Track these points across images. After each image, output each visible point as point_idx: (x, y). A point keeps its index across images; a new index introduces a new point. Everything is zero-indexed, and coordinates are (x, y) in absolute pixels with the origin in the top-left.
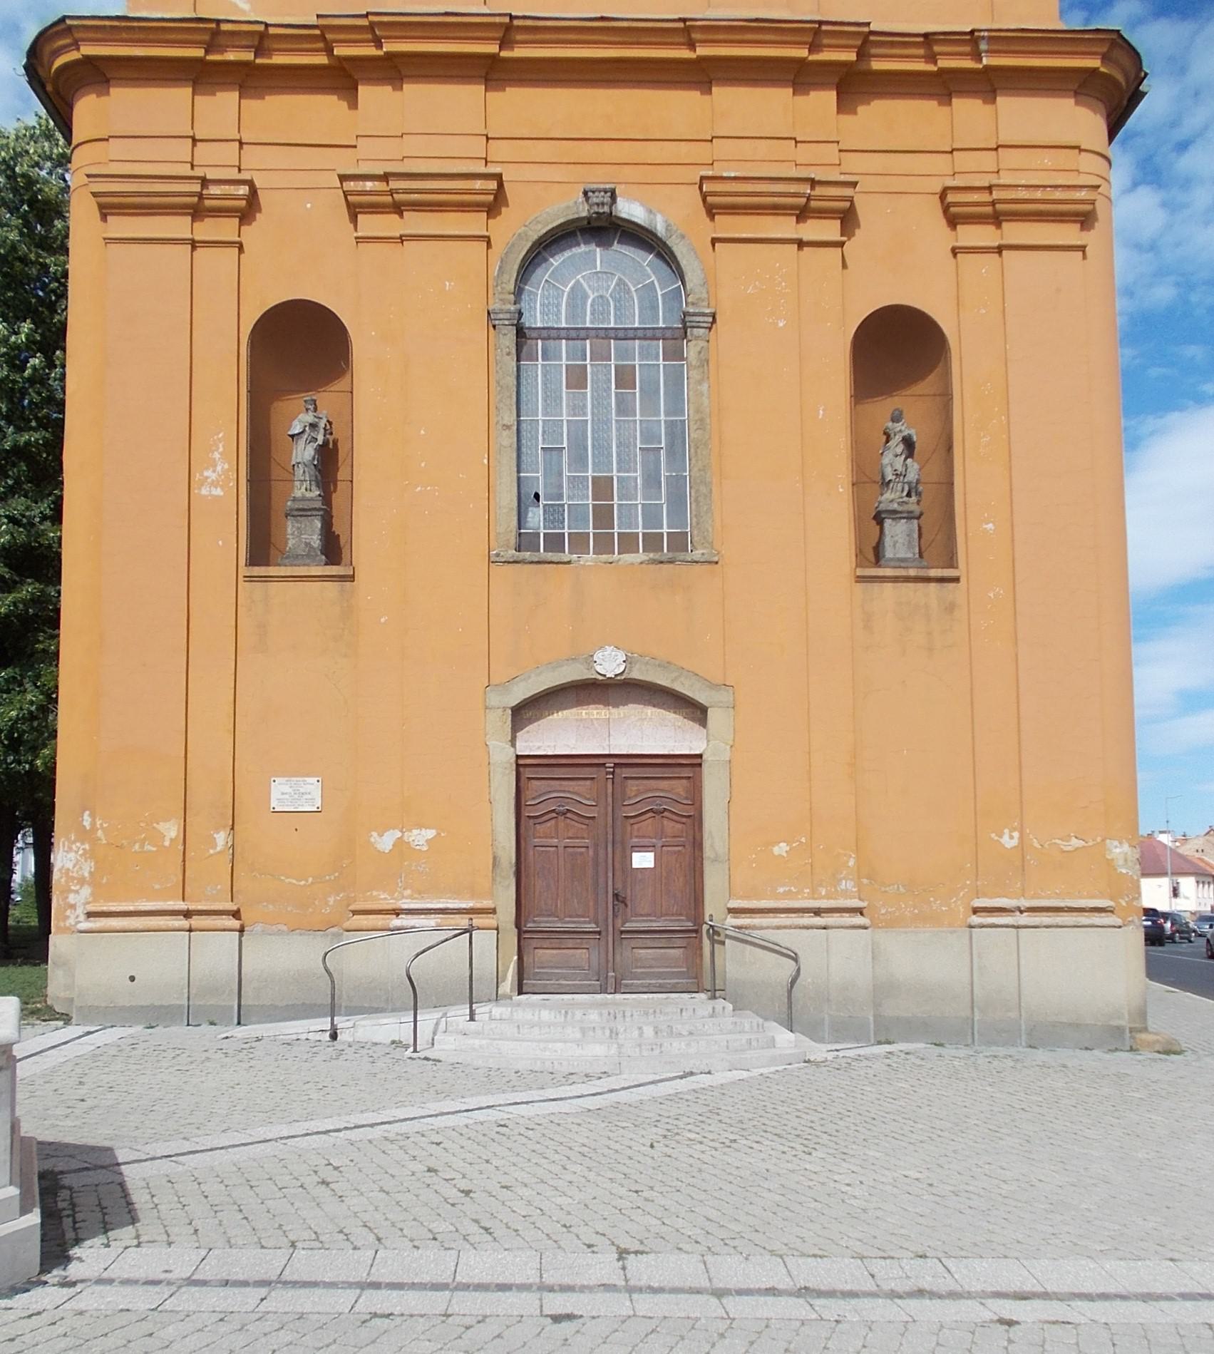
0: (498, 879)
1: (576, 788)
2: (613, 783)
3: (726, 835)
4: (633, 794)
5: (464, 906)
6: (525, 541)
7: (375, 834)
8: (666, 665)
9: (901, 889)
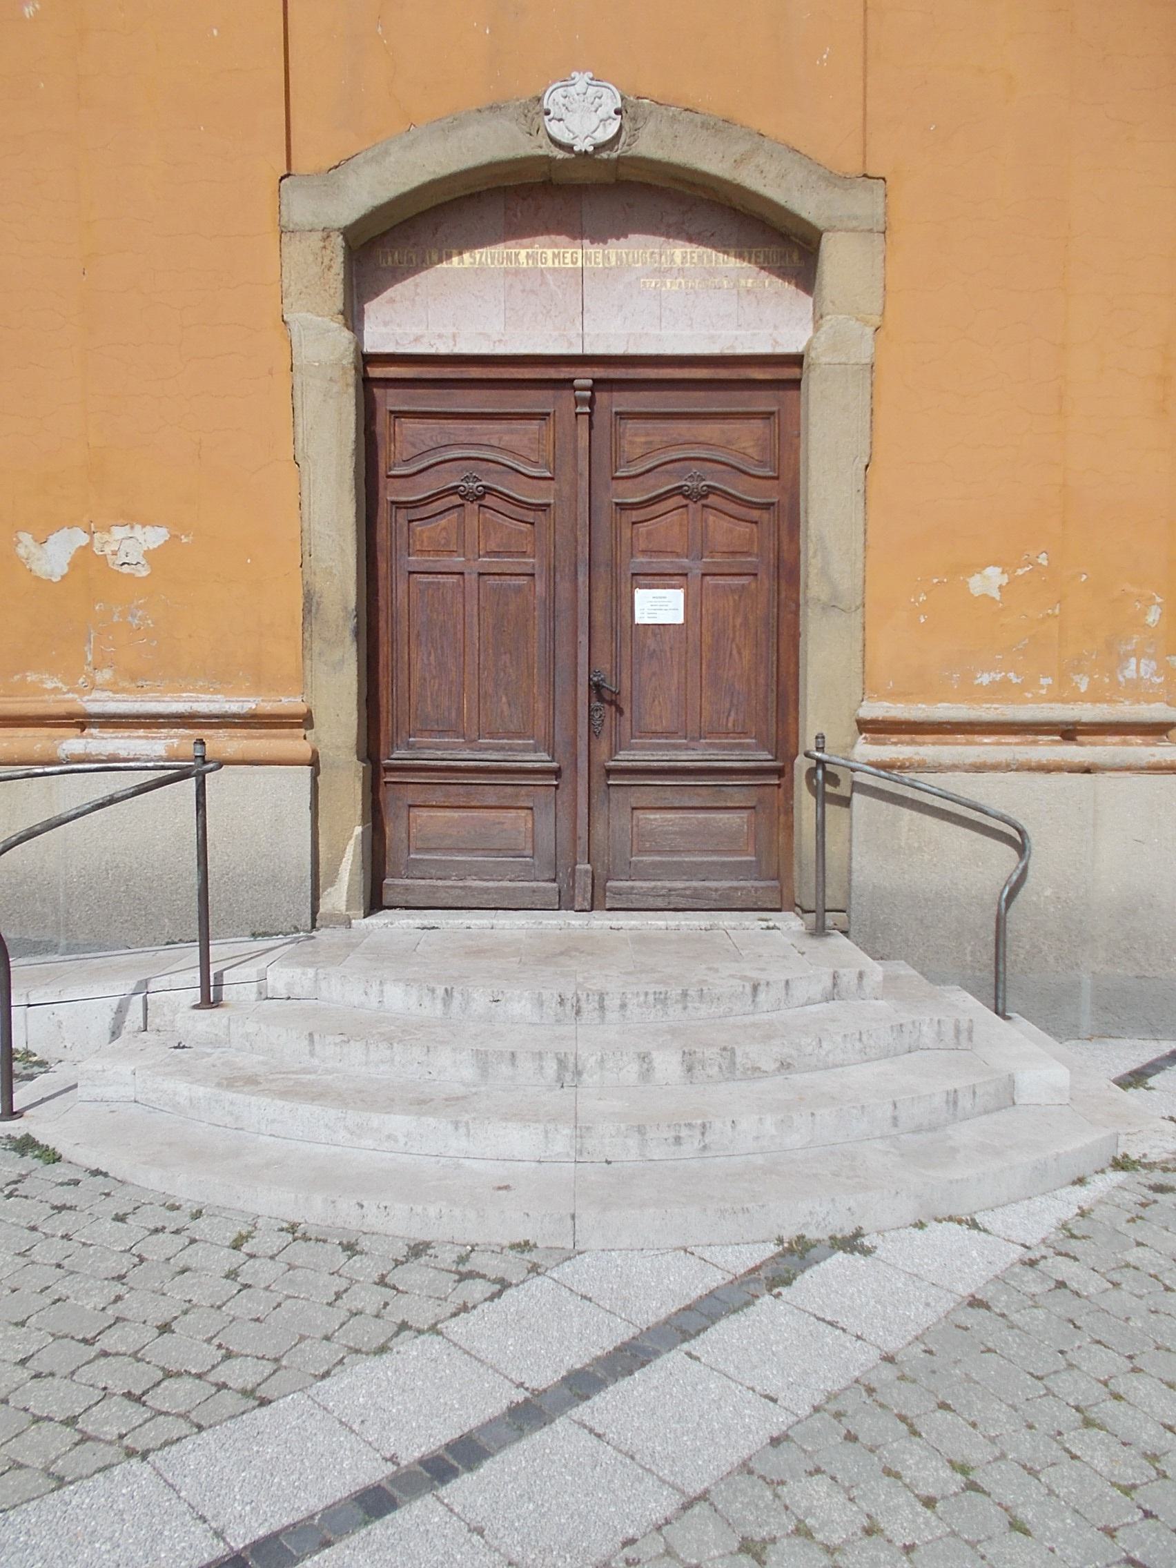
0: (317, 646)
1: (506, 438)
2: (591, 427)
3: (860, 545)
4: (639, 451)
5: (234, 707)
7: (26, 538)
8: (722, 126)
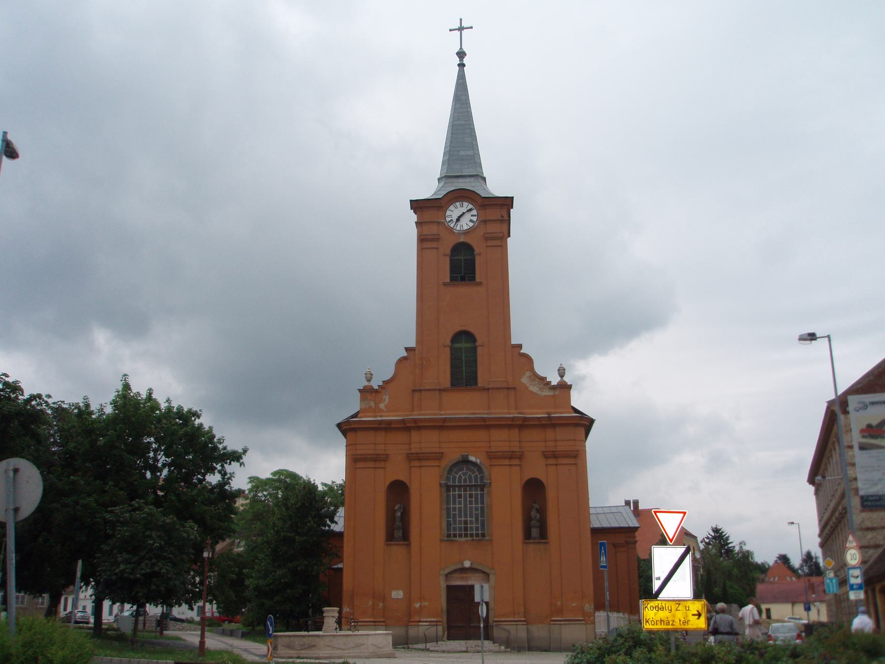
6: (449, 536)
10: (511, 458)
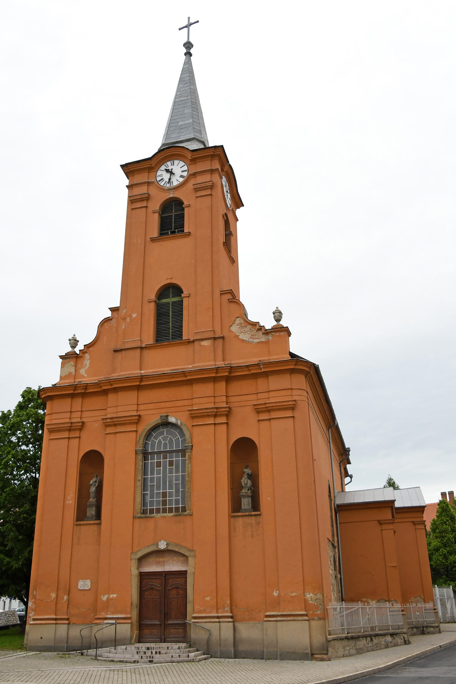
6: (144, 512)
7: (102, 596)
8: (177, 545)
9: (245, 610)
10: (215, 416)
